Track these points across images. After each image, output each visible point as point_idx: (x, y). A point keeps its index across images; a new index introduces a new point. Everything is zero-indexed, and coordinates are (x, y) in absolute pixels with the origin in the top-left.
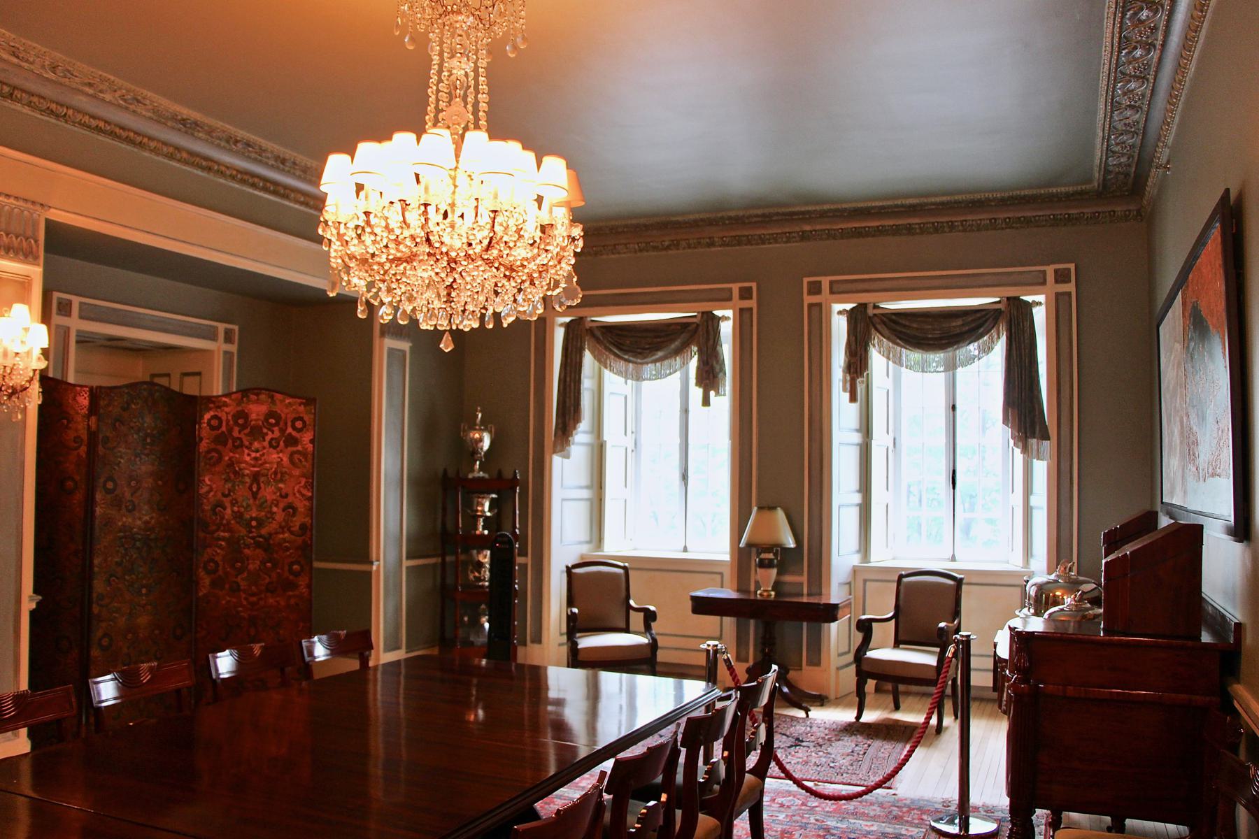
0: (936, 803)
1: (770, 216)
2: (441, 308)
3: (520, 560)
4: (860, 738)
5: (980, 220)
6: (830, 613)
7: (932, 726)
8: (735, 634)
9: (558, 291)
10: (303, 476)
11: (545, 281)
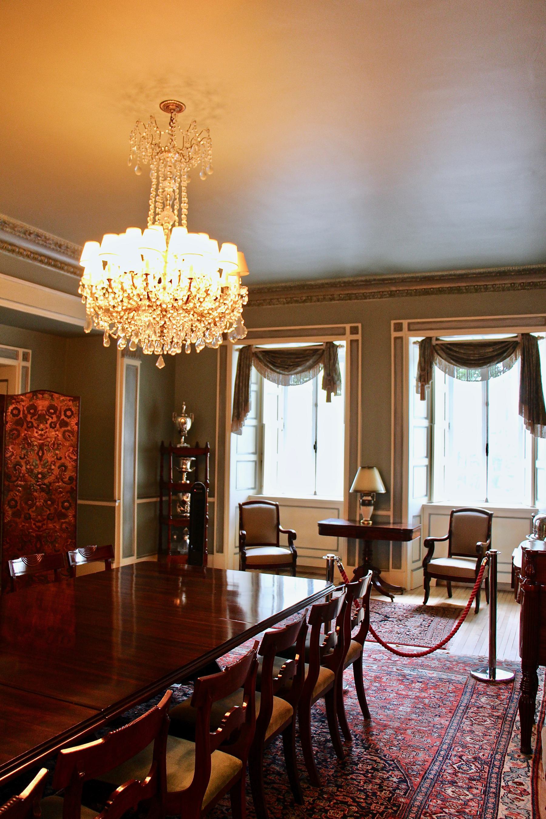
0: (474, 659)
1: (370, 281)
2: (157, 340)
3: (209, 499)
4: (426, 616)
5: (505, 284)
6: (407, 535)
7: (473, 609)
8: (347, 547)
9: (231, 330)
10: (71, 446)
11: (224, 323)
